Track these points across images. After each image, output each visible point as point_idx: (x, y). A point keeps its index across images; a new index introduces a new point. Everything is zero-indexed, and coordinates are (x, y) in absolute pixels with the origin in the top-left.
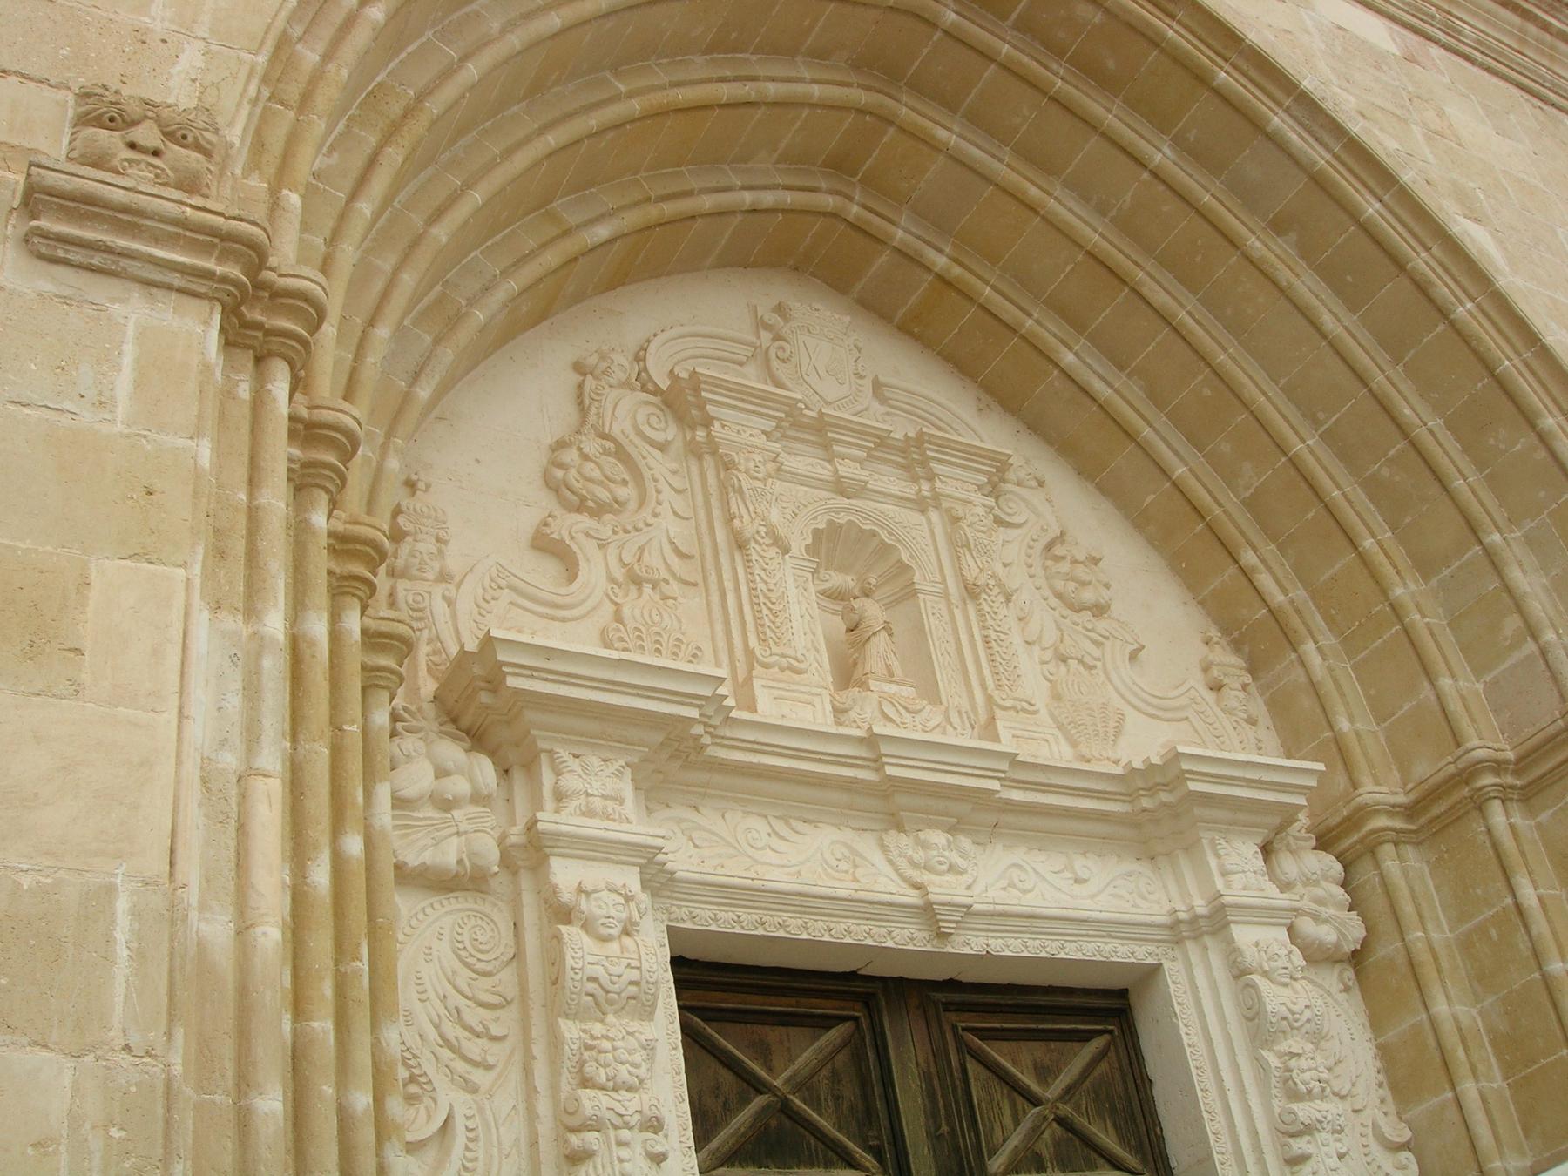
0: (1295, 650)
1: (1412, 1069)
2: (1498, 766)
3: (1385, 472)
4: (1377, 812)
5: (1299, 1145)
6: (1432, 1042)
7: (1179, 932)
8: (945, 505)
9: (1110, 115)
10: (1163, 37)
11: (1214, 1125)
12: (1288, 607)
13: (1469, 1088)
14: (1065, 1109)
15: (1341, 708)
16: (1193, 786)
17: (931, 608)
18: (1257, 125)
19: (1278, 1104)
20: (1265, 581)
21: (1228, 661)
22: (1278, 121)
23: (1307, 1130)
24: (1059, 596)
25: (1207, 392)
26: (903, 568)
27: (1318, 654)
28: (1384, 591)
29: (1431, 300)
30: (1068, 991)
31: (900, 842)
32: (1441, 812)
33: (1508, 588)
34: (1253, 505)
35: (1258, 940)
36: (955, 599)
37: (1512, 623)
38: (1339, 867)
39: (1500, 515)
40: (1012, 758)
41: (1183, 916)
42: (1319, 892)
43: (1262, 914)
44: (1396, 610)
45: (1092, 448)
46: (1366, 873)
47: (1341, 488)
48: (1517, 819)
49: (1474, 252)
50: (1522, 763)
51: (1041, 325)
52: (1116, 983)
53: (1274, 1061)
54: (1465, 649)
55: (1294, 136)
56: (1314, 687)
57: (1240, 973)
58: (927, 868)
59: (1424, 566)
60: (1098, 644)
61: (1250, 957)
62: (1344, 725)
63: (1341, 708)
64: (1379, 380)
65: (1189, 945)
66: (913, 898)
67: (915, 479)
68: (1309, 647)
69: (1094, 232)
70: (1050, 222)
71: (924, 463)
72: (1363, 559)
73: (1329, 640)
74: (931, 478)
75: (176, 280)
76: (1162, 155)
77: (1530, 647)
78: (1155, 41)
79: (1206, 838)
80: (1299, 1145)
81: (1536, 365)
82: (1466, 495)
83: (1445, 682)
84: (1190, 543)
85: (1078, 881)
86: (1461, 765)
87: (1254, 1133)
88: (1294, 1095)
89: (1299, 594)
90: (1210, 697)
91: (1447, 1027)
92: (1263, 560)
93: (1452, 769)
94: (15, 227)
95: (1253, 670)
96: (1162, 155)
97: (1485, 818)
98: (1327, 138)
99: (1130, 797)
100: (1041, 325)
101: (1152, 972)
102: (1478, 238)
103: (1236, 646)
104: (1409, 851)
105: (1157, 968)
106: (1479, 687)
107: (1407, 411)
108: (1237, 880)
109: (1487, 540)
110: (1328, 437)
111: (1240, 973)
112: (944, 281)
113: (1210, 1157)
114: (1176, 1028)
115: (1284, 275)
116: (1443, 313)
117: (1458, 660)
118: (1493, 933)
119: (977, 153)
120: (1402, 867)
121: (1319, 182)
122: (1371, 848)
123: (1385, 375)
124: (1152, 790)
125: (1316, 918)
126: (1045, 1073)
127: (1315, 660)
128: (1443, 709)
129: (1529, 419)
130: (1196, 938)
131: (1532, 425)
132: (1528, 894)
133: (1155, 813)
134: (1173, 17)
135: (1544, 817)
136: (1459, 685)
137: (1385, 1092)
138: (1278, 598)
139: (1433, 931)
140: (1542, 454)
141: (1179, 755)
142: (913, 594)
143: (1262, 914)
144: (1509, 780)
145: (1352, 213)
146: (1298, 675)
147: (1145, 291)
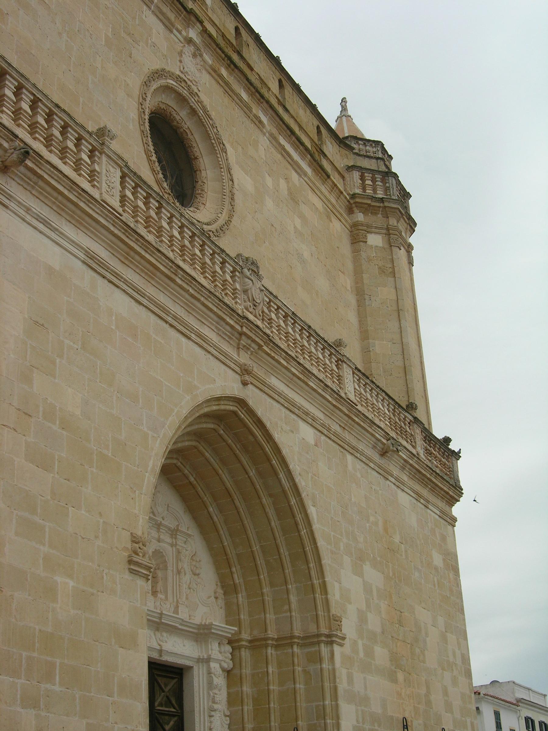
0: (236, 594)
1: (234, 700)
2: (273, 639)
3: (271, 561)
4: (243, 641)
5: (213, 713)
6: (240, 695)
7: (199, 660)
8: (177, 547)
9: (244, 460)
10: (265, 449)
11: (196, 705)
12: (238, 584)
13: (246, 708)
14: (168, 694)
15: (242, 613)
16: (213, 631)
17: (170, 572)
18: (276, 474)
19: (210, 703)
20: (235, 576)
21: (220, 591)
22: (282, 475)
23: (215, 710)
24: (192, 571)
25: (239, 527)
26: (165, 561)
27: (241, 598)
28: (261, 588)
29: (297, 527)
30: (173, 667)
31: (158, 634)
32: (257, 645)
33: (288, 598)
34: (238, 555)
35: (214, 665)
36: (175, 573)
37: (286, 607)
38: (231, 650)
39: (293, 579)
40: (182, 620)
41: (201, 658)
42: (226, 655)
43: (217, 661)
44: (262, 594)
45: (206, 529)
46: (237, 653)
47: (260, 561)
48: (273, 652)
49: (311, 519)
50: (277, 640)
51: (207, 499)
52: (181, 667)
53: (212, 694)
54: (274, 607)
55: (284, 481)
56: (238, 605)
57: (209, 673)
58: (162, 641)
59: (272, 585)
60: (197, 585)
61: (213, 670)
62: (242, 617)
63: (242, 613)
64: (279, 541)
65: (200, 664)
66: (158, 647)
67: (172, 538)
68: (240, 595)
69: (229, 483)
70: (221, 479)
71: (176, 535)
72: (259, 579)
73: (244, 594)
74: (176, 538)
75: (143, 575)
76: (252, 473)
77: (288, 614)
78: (262, 448)
79: (210, 640)
80: (213, 713)
81: (314, 550)
82: (287, 574)
83: (268, 615)
84: (221, 561)
85: (184, 646)
86: (265, 636)
87: (204, 708)
88: (214, 702)
89: (241, 580)
90: (214, 600)
91: (245, 693)
92: (236, 571)
93: (263, 637)
94: (127, 566)
95: (225, 594)
96: (252, 473)
97: (266, 649)
98: (290, 481)
99: (198, 629)
100: (207, 499)
101: (190, 668)
102: (312, 511)
103: (223, 587)
104: (247, 650)
105: (193, 667)
106: (274, 617)
107: (282, 550)
108: (214, 652)
109: (288, 586)
110: (261, 547)
111: (209, 673)
112: (191, 483)
113: (194, 711)
114: (193, 683)
115: (268, 510)
116: (299, 531)
117: (272, 610)
118: (260, 675)
119: (212, 460)
120: (245, 654)
121: (284, 491)
122: (239, 648)
123: (281, 540)
124: (204, 629)
125: (225, 661)
126: (166, 685)
127: (240, 599)
128: (265, 621)
129: (307, 562)
130: (202, 662)
131: (308, 564)
132: (270, 670)
133: (202, 634)
134: (268, 443)
135: (278, 653)
136: (270, 617)
137: (226, 703)
138: (237, 581)
139: (247, 671)
140: (307, 571)
141: (213, 624)
142: (167, 569)
143: (217, 661)
144: (274, 643)
145: (289, 502)
146: (235, 600)
147: (235, 501)
